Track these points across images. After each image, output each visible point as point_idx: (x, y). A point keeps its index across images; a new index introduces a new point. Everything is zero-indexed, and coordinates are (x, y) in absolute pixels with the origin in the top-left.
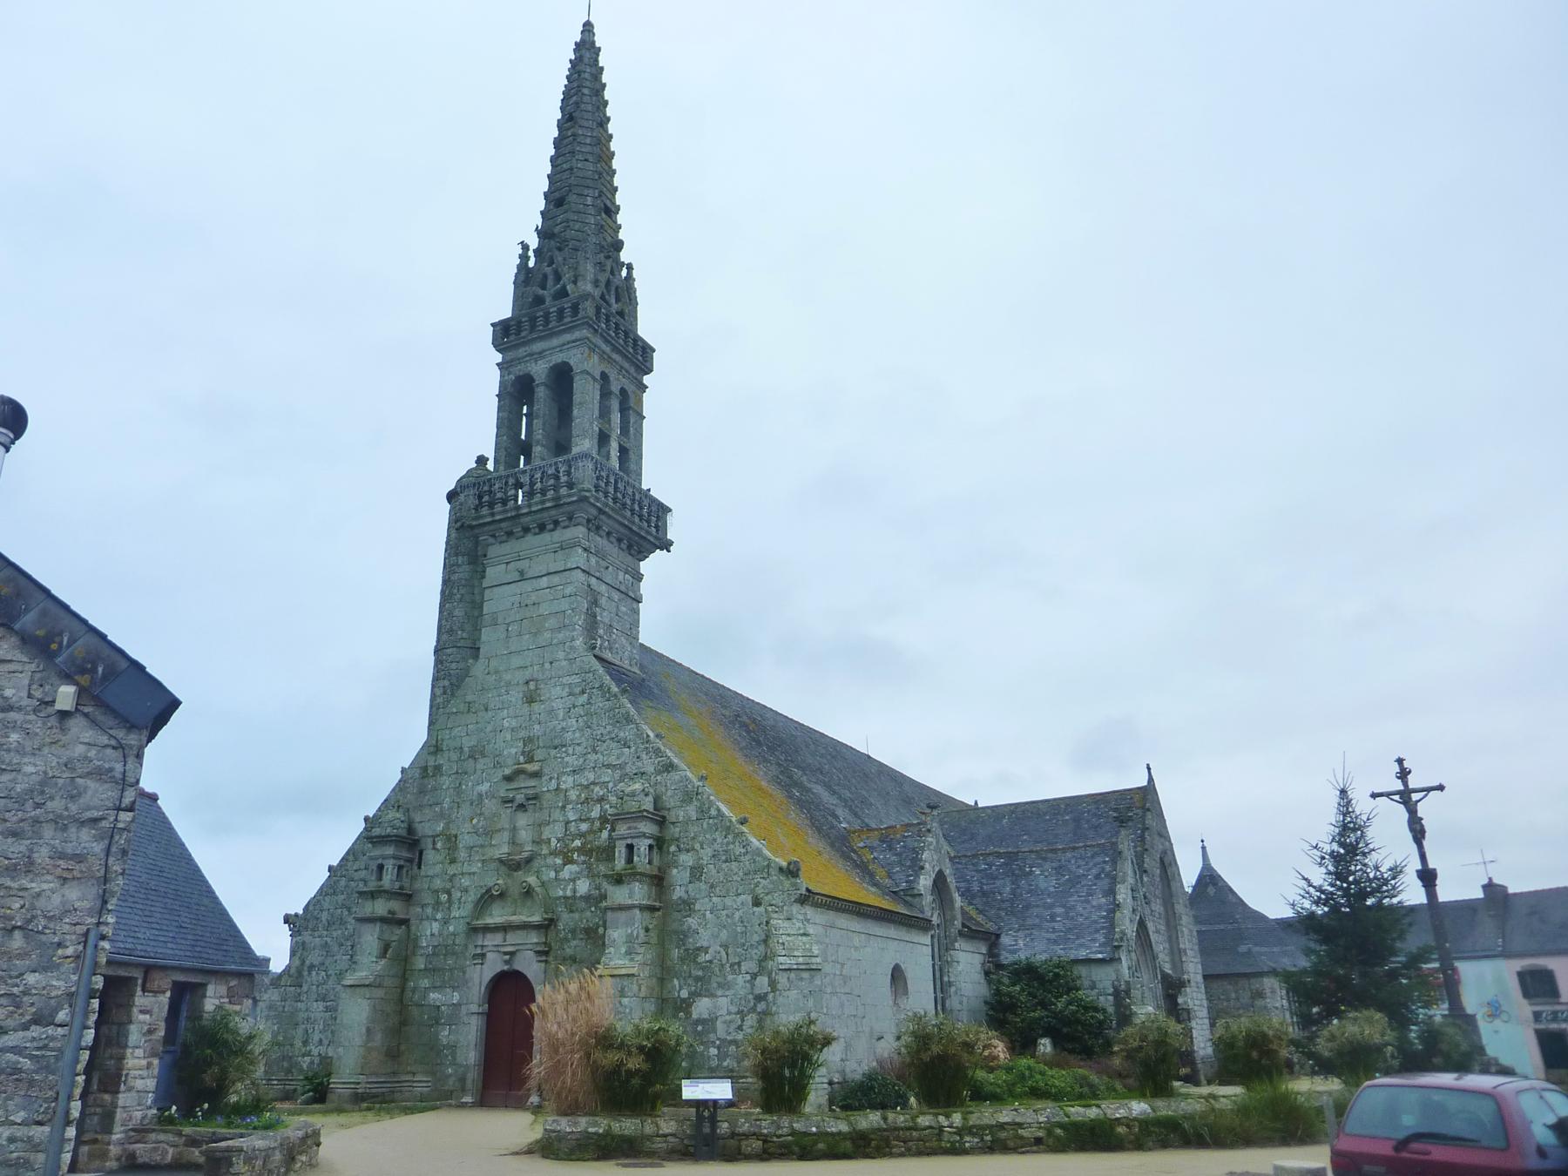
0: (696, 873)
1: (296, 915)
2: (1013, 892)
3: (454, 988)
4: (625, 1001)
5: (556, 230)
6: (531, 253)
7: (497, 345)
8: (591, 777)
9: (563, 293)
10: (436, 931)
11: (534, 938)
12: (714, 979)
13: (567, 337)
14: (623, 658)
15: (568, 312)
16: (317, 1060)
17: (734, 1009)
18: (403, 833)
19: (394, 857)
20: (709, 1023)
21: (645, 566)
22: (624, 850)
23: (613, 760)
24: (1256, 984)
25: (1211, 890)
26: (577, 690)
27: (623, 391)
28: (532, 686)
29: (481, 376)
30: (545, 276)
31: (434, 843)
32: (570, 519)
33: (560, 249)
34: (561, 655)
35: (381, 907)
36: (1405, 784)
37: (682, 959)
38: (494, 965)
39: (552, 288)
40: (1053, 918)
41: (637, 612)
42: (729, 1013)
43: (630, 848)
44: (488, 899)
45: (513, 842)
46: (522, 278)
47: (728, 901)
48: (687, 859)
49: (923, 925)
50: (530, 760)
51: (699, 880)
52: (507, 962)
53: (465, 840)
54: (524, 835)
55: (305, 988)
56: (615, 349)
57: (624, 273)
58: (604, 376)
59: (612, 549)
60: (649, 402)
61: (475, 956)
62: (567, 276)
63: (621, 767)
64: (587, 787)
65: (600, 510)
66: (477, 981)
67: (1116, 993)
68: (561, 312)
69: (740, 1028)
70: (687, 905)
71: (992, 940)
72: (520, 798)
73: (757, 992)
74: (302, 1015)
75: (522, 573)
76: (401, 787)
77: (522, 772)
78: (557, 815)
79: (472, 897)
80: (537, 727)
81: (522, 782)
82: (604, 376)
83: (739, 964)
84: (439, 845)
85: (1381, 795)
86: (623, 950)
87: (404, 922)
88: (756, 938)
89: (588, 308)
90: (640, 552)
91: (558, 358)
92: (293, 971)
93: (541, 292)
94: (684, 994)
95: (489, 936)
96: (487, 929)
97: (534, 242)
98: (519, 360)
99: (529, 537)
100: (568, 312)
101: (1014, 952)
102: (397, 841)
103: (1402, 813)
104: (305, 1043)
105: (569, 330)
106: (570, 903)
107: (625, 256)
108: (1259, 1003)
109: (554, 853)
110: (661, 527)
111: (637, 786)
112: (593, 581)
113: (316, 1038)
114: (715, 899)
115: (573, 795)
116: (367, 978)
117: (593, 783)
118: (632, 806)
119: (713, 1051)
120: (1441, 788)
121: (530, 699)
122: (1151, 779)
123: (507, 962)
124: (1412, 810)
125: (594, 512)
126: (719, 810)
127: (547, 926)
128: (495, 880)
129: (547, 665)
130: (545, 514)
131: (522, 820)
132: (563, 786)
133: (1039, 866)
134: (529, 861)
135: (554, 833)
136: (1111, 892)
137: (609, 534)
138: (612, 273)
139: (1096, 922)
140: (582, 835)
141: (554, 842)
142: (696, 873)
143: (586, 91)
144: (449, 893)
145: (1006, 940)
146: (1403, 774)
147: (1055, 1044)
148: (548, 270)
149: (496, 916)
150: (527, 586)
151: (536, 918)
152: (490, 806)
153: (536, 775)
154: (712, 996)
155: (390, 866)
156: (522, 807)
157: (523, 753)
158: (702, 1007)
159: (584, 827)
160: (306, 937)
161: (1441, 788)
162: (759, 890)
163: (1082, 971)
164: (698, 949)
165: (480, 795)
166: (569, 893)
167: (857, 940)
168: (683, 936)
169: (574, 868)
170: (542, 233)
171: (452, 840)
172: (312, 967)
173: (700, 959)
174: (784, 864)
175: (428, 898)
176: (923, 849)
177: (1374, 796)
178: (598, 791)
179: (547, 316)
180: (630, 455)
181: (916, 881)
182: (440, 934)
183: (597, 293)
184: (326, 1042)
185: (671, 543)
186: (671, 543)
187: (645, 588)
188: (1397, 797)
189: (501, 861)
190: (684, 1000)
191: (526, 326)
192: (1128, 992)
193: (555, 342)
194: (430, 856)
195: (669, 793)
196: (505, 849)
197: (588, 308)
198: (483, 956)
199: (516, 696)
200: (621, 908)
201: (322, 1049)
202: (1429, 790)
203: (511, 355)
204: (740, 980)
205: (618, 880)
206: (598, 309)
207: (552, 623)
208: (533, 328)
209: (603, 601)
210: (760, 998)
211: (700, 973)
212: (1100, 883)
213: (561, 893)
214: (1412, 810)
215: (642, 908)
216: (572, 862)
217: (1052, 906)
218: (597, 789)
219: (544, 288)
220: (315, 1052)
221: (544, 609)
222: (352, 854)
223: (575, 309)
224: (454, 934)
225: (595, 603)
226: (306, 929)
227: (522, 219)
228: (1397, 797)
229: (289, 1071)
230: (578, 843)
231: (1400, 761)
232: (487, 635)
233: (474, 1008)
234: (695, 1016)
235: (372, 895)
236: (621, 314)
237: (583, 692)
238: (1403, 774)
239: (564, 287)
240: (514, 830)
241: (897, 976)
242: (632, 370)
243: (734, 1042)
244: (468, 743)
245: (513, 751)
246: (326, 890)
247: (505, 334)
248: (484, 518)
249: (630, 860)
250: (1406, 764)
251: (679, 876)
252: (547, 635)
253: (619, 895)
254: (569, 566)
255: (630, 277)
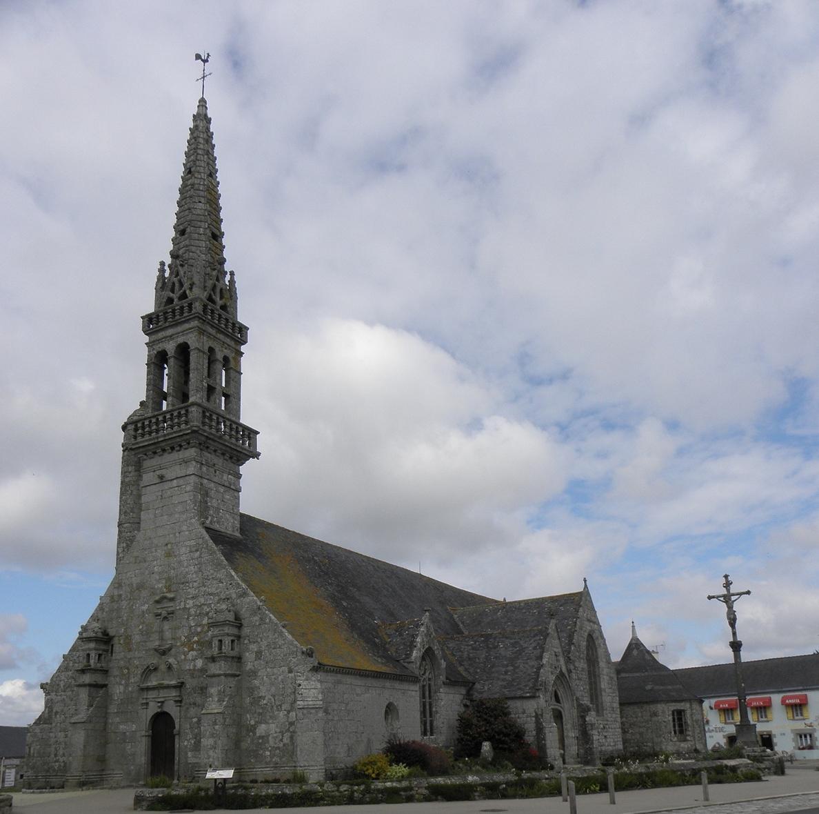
0: (259, 654)
1: (47, 684)
2: (486, 658)
3: (133, 722)
4: (217, 727)
5: (181, 252)
6: (166, 268)
7: (147, 331)
8: (202, 600)
9: (184, 296)
10: (122, 690)
11: (174, 693)
12: (268, 714)
13: (187, 326)
14: (230, 527)
15: (186, 309)
16: (62, 764)
17: (278, 730)
18: (100, 635)
19: (95, 649)
20: (264, 738)
21: (243, 469)
22: (217, 643)
23: (213, 590)
24: (653, 707)
25: (635, 652)
26: (194, 549)
27: (226, 359)
28: (169, 546)
29: (138, 349)
30: (174, 283)
31: (119, 640)
32: (189, 443)
33: (182, 266)
34: (184, 528)
35: (87, 678)
36: (728, 591)
37: (251, 704)
38: (153, 709)
39: (178, 293)
40: (506, 673)
41: (238, 498)
42: (276, 733)
43: (220, 641)
44: (149, 671)
45: (162, 639)
46: (160, 285)
47: (275, 671)
48: (254, 647)
49: (414, 679)
50: (170, 591)
51: (260, 659)
52: (159, 707)
53: (137, 638)
54: (168, 634)
55: (54, 725)
56: (219, 331)
57: (228, 278)
58: (211, 350)
59: (219, 461)
60: (245, 363)
61: (142, 704)
62: (186, 285)
63: (218, 594)
64: (200, 606)
65: (207, 437)
66: (144, 718)
67: (537, 716)
68: (182, 308)
69: (281, 740)
70: (254, 673)
71: (469, 686)
72: (164, 613)
73: (290, 720)
74: (53, 740)
75: (161, 477)
76: (101, 608)
77: (165, 598)
78: (184, 622)
79: (140, 671)
80: (172, 571)
81: (166, 604)
82: (211, 350)
83: (281, 706)
84: (122, 642)
85: (713, 597)
86: (216, 699)
87: (105, 686)
88: (290, 691)
89: (198, 307)
90: (238, 460)
91: (181, 340)
92: (46, 715)
93: (171, 295)
94: (253, 722)
95: (150, 692)
96: (148, 689)
97: (168, 261)
98: (160, 341)
99: (166, 455)
100: (186, 309)
101: (482, 693)
102: (96, 640)
103: (724, 607)
104: (56, 755)
105: (187, 321)
106: (192, 673)
107: (227, 267)
108: (655, 719)
109: (183, 645)
110: (253, 444)
111: (224, 607)
112: (205, 481)
113: (61, 752)
114: (268, 669)
115: (192, 611)
116: (83, 718)
117: (203, 604)
118: (221, 618)
119: (268, 753)
120: (748, 593)
121: (168, 555)
122: (586, 586)
123: (159, 707)
124: (730, 608)
125: (203, 439)
126: (270, 619)
127: (180, 686)
128: (154, 660)
129: (177, 534)
130: (173, 441)
131: (166, 626)
132: (188, 606)
133: (502, 642)
134: (170, 649)
135: (183, 634)
136: (541, 657)
137: (215, 451)
138: (218, 280)
139: (529, 675)
140: (198, 634)
141: (183, 638)
142: (259, 654)
143: (200, 152)
144: (128, 669)
145: (477, 686)
146: (727, 585)
147: (494, 748)
148: (175, 280)
149: (153, 682)
150: (166, 485)
151: (173, 682)
152: (149, 618)
153: (172, 599)
154: (266, 723)
155: (93, 654)
156: (165, 618)
157: (165, 587)
158: (262, 729)
159: (199, 629)
160: (53, 695)
161: (748, 593)
162: (291, 664)
163: (510, 703)
164: (260, 697)
165: (143, 612)
166: (191, 668)
167: (358, 690)
168: (252, 690)
169: (194, 653)
170: (174, 255)
171: (128, 638)
172: (56, 713)
173: (260, 703)
174: (305, 649)
175: (116, 672)
176: (417, 635)
177: (710, 598)
178: (206, 609)
179: (173, 311)
180: (232, 396)
181: (410, 655)
182: (124, 692)
183: (204, 295)
184: (66, 754)
185: (259, 454)
186: (259, 454)
187: (243, 483)
188: (722, 599)
189: (156, 650)
190: (252, 726)
191: (161, 318)
192: (542, 715)
193: (179, 329)
194: (117, 648)
195: (244, 610)
196: (157, 643)
197: (198, 307)
198: (147, 704)
199: (160, 553)
200: (214, 676)
201: (65, 759)
202: (741, 594)
203: (154, 337)
204: (281, 714)
205: (213, 659)
206: (205, 307)
207: (179, 508)
208: (166, 319)
209: (212, 493)
210: (292, 724)
211: (261, 711)
212: (535, 652)
213: (188, 668)
214: (730, 608)
215: (226, 675)
216: (193, 649)
217: (507, 666)
218: (206, 607)
219: (173, 292)
220: (61, 760)
221: (176, 500)
222: (73, 649)
223: (190, 306)
224: (132, 692)
225: (207, 494)
226: (52, 692)
227: (159, 245)
228: (722, 599)
229: (48, 771)
230: (196, 638)
231: (726, 577)
232: (143, 515)
233: (143, 733)
234: (258, 735)
235: (83, 671)
236: (224, 307)
237: (197, 551)
238: (727, 585)
239: (185, 292)
240: (161, 632)
241: (390, 710)
242: (232, 344)
243: (279, 748)
244: (135, 581)
245: (160, 586)
246: (63, 668)
247: (152, 323)
248: (146, 439)
249: (220, 649)
250: (729, 578)
251: (249, 656)
252: (177, 516)
253: (214, 668)
254: (188, 473)
255: (232, 282)
